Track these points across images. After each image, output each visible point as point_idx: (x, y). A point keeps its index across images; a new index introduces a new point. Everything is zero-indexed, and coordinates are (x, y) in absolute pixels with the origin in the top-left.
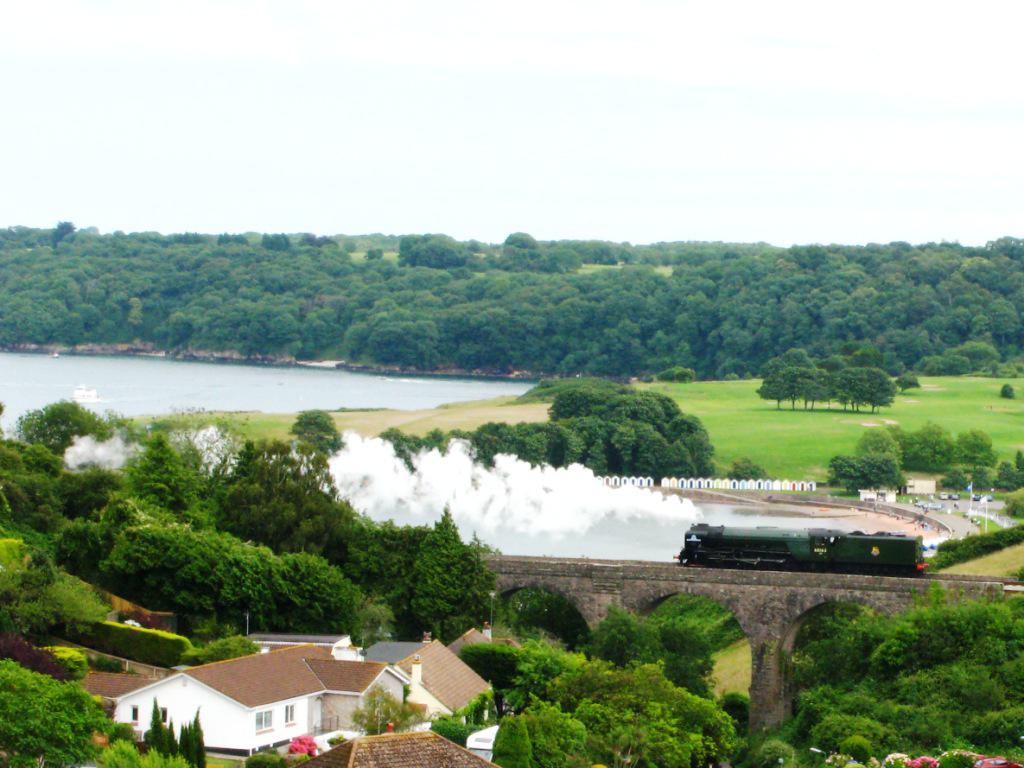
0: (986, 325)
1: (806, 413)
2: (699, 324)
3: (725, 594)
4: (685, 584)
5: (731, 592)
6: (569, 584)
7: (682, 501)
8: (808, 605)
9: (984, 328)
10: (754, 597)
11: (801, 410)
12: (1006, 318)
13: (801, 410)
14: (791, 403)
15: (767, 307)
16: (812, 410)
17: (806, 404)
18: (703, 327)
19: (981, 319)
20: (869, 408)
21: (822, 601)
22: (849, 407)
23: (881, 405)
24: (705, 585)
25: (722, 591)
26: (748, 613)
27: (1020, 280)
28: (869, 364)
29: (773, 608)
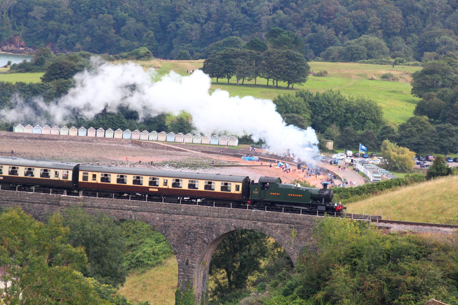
0: (378, 24)
1: (237, 87)
2: (160, 18)
3: (160, 220)
4: (130, 212)
5: (164, 220)
6: (42, 209)
7: (244, 132)
8: (222, 232)
9: (377, 27)
10: (182, 225)
11: (235, 85)
12: (394, 20)
13: (235, 85)
14: (266, 80)
15: (212, 5)
16: (243, 85)
17: (289, 85)
18: (163, 20)
19: (374, 18)
20: (285, 84)
21: (233, 229)
22: (271, 83)
23: (296, 82)
24: (145, 214)
25: (158, 218)
26: (176, 236)
27: (454, 144)
28: (228, 36)
29: (196, 233)
